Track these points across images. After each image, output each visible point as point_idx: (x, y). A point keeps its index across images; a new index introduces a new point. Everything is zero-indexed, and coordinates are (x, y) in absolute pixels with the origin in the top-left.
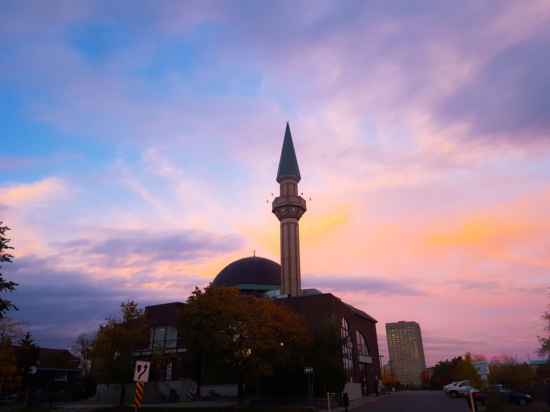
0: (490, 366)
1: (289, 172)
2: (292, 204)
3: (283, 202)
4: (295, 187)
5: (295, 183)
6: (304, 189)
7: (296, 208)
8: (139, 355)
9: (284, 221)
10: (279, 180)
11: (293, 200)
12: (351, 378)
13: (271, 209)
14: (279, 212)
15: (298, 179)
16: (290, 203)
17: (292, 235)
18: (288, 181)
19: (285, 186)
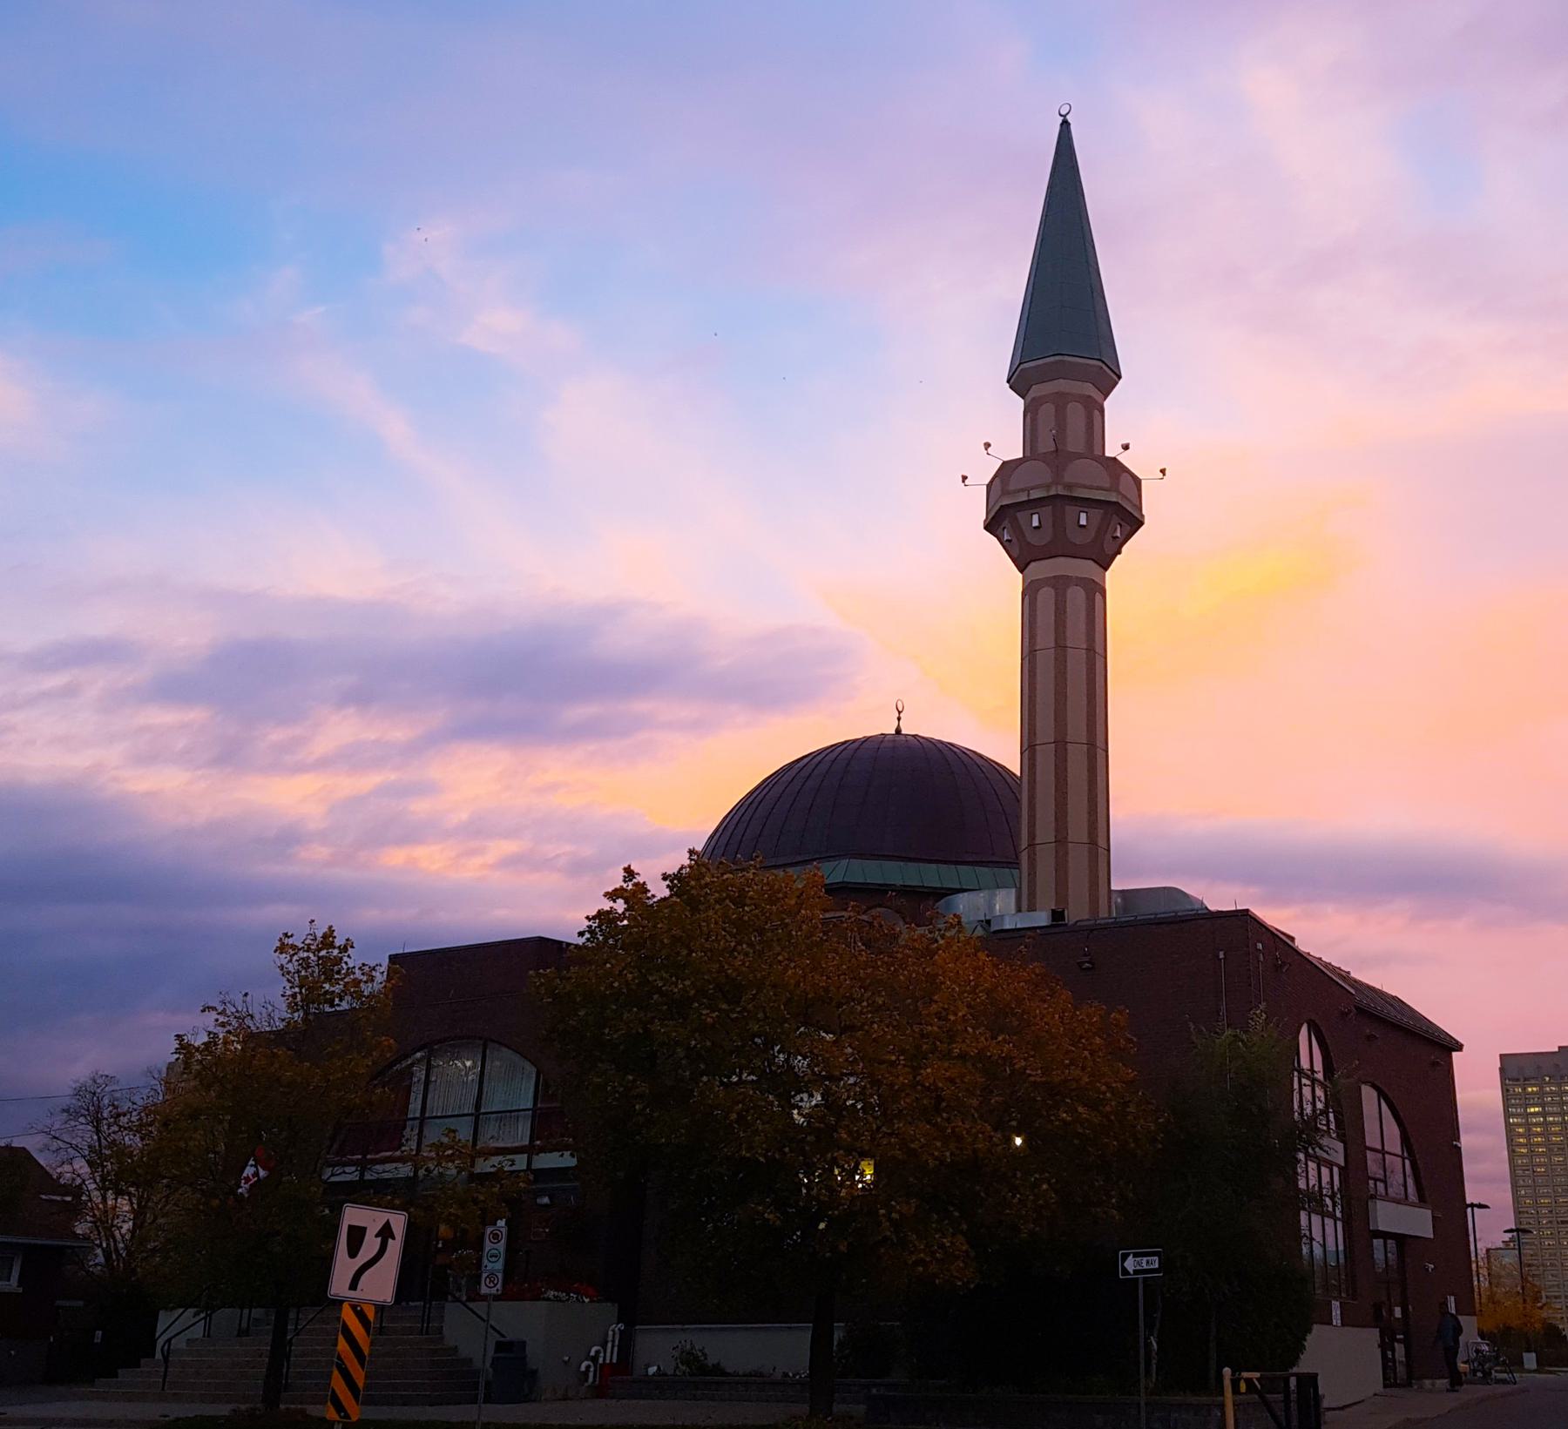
3: (1038, 483)
6: (1132, 426)
7: (1097, 513)
9: (1040, 569)
11: (1082, 476)
14: (1018, 530)
15: (1108, 376)
16: (1069, 487)
19: (1048, 410)
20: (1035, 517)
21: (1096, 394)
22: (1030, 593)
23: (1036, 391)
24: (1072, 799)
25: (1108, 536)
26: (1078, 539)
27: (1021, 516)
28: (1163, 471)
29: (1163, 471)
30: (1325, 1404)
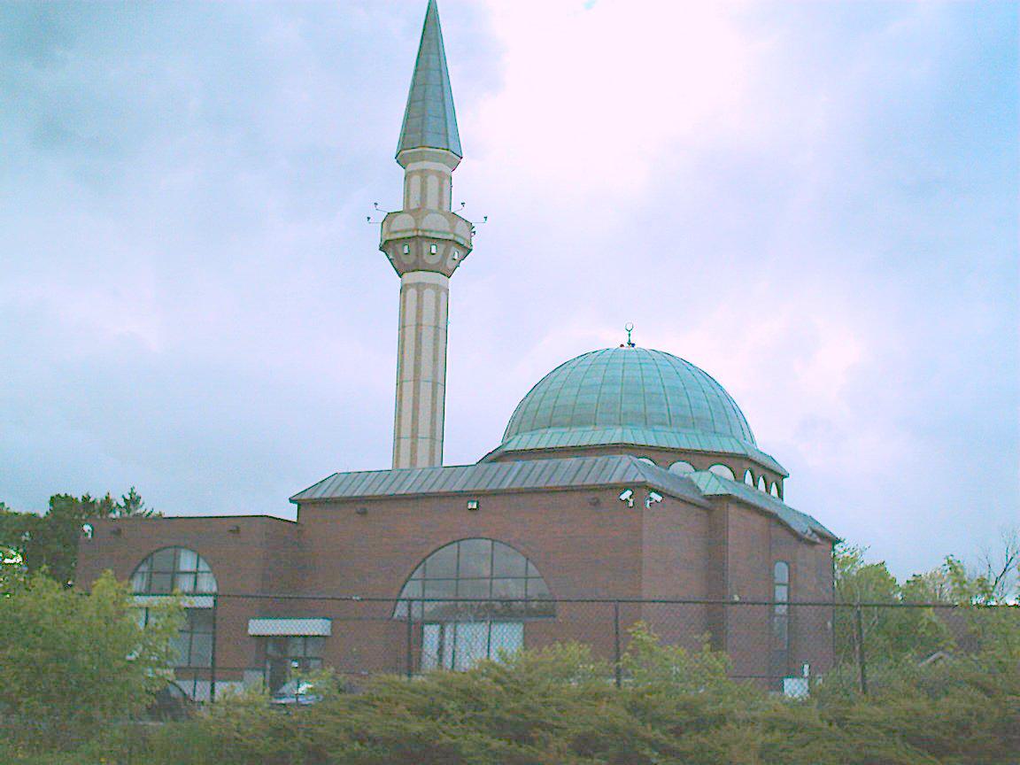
0: (726, 650)
1: (428, 130)
2: (427, 234)
3: (404, 224)
4: (445, 180)
5: (447, 170)
6: (472, 189)
7: (442, 246)
8: (221, 687)
9: (410, 277)
10: (401, 159)
11: (434, 223)
12: (258, 627)
13: (377, 242)
14: (396, 254)
15: (455, 157)
16: (423, 231)
17: (428, 319)
18: (426, 165)
19: (416, 180)
20: (406, 247)
21: (447, 170)
22: (403, 290)
23: (411, 167)
24: (409, 416)
25: (450, 258)
26: (432, 261)
27: (454, 249)
28: (486, 218)
29: (486, 218)
30: (776, 581)
